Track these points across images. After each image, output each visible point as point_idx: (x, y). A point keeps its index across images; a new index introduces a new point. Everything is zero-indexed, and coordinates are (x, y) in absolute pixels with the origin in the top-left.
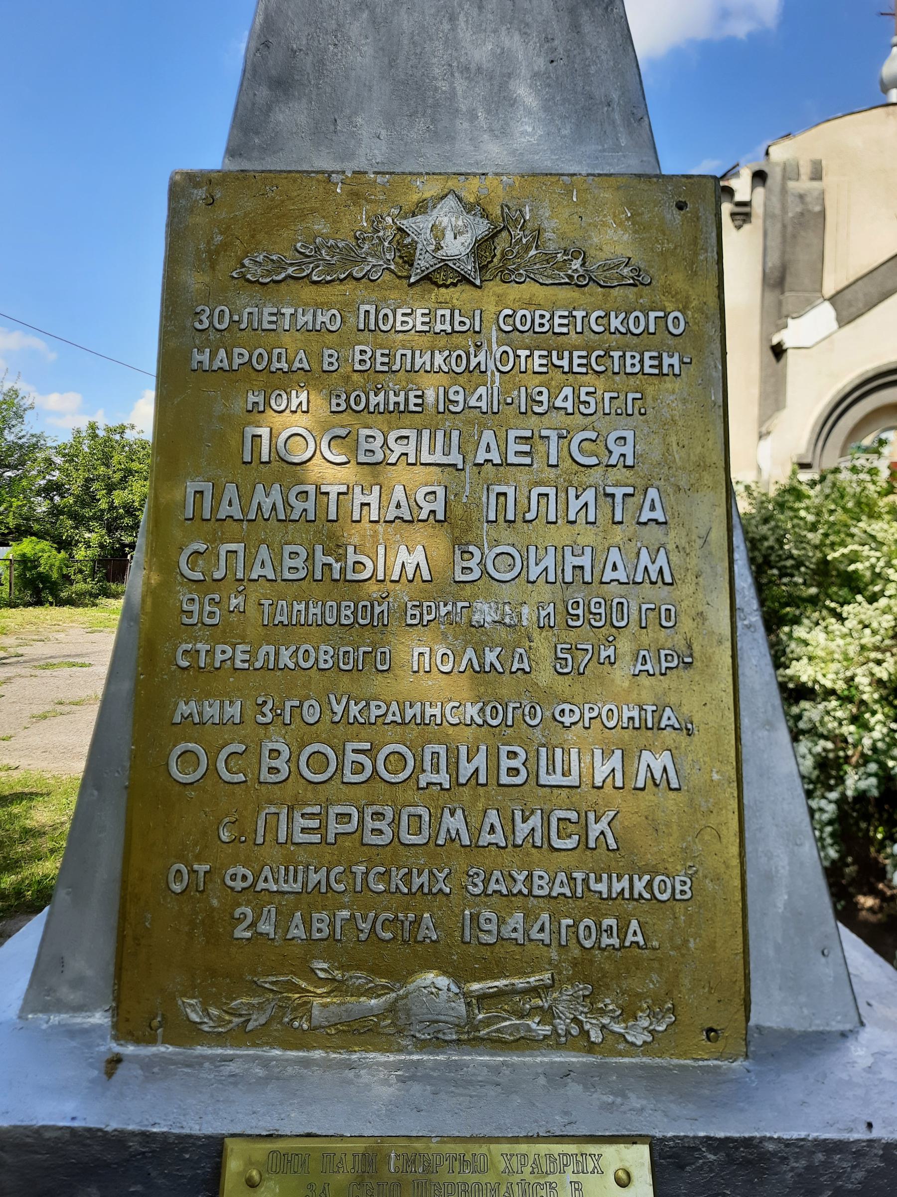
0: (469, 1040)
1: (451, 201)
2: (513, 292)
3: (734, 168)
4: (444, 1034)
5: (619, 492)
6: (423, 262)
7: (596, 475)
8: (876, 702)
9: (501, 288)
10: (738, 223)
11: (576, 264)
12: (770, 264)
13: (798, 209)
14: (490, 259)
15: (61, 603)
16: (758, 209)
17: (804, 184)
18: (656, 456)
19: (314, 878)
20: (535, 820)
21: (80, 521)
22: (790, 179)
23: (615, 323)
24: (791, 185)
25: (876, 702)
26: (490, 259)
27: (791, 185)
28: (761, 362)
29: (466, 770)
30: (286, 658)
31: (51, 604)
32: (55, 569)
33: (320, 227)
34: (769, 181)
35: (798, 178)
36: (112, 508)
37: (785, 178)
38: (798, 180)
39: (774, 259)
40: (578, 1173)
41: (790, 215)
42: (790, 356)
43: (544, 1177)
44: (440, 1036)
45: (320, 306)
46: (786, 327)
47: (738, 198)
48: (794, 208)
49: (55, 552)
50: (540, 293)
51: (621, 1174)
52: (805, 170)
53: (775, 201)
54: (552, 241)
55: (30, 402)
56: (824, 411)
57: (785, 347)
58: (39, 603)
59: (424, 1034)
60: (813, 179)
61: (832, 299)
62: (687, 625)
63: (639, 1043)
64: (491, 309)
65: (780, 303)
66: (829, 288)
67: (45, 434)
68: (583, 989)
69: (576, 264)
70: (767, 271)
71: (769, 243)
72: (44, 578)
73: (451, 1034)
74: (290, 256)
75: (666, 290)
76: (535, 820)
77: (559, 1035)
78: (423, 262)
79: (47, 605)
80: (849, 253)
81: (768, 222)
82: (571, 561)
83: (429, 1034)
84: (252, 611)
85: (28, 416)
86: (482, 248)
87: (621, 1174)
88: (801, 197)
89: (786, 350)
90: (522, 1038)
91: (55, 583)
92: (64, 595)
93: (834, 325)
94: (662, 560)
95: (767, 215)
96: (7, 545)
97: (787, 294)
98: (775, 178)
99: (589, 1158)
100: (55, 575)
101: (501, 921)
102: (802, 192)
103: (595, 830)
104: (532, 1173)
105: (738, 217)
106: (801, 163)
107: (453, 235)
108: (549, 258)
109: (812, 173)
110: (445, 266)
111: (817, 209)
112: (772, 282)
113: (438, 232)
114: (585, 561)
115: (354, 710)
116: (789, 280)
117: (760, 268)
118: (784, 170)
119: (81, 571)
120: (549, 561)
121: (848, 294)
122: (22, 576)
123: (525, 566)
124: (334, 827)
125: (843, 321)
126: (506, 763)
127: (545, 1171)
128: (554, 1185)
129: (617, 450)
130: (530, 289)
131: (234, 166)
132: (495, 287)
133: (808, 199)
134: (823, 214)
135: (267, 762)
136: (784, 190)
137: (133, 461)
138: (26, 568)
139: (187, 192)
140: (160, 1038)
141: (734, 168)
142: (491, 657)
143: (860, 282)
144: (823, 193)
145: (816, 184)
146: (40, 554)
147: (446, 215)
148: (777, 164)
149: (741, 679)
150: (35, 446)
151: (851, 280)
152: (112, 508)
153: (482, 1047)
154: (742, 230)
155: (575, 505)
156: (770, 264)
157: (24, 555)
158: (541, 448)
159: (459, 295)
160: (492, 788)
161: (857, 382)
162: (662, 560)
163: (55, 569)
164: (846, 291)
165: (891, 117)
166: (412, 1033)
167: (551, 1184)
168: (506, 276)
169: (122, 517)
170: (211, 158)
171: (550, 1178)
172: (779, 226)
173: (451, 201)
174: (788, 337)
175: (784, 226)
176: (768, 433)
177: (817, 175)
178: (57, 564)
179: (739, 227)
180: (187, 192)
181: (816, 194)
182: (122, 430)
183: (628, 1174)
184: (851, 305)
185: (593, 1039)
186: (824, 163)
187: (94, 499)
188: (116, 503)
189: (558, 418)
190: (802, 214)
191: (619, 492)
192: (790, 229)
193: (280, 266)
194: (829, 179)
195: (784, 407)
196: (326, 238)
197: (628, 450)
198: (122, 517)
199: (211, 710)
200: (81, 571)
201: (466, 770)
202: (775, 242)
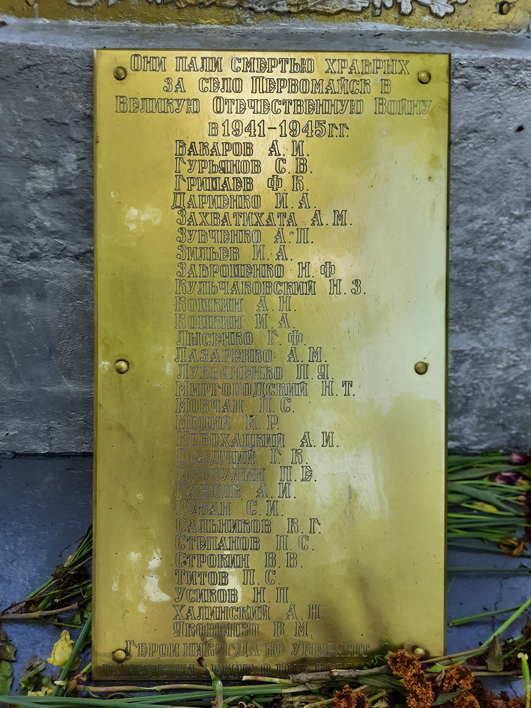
0: (299, 13)
4: (277, 6)
8: (525, 211)
25: (525, 211)
40: (388, 73)
43: (360, 76)
44: (274, 7)
51: (423, 75)
59: (260, 6)
63: (442, 14)
73: (283, 5)
77: (375, 8)
83: (264, 7)
87: (423, 75)
90: (344, 10)
99: (398, 63)
104: (350, 73)
127: (361, 71)
128: (368, 82)
140: (37, 12)
149: (452, 120)
153: (309, 20)
166: (250, 5)
167: (365, 81)
171: (365, 77)
183: (430, 76)
185: (403, 10)
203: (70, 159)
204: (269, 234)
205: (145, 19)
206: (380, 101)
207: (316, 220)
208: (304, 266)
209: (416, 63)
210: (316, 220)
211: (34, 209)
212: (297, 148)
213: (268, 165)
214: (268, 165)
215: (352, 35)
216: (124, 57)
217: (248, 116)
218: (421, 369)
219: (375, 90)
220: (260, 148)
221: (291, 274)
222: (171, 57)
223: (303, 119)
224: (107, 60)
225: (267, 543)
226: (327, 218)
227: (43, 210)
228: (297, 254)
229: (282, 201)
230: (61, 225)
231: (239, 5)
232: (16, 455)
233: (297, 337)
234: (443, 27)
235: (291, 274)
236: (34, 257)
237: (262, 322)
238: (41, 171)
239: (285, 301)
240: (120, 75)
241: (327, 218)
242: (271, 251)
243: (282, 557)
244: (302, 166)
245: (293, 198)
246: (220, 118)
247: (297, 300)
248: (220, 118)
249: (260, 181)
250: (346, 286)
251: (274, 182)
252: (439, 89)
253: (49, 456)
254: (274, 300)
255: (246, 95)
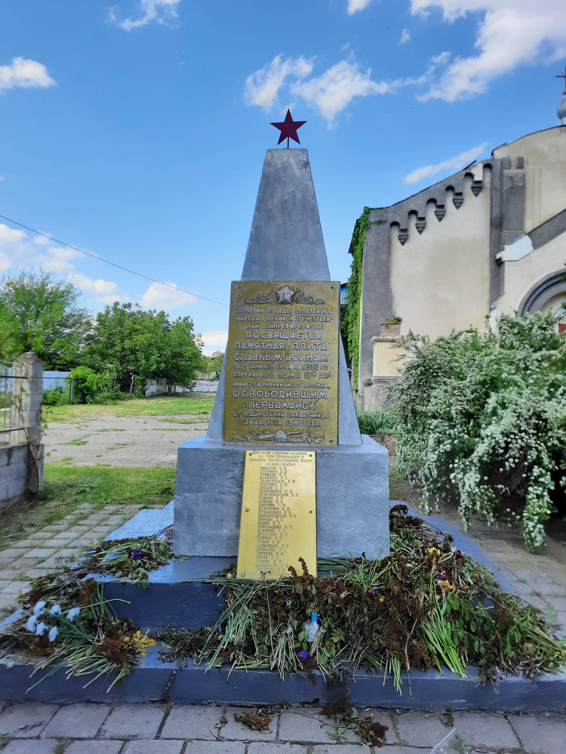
1: (287, 287)
2: (298, 305)
3: (473, 163)
5: (318, 344)
6: (281, 300)
7: (313, 341)
9: (296, 305)
10: (476, 193)
11: (311, 300)
12: (494, 215)
13: (510, 185)
14: (294, 299)
15: (98, 403)
16: (487, 183)
17: (513, 171)
18: (325, 337)
19: (259, 414)
20: (300, 404)
21: (104, 357)
22: (505, 168)
23: (318, 311)
24: (506, 171)
26: (294, 299)
27: (506, 171)
28: (490, 269)
29: (287, 395)
30: (254, 375)
31: (91, 403)
32: (95, 384)
33: (261, 292)
34: (494, 170)
35: (510, 167)
36: (123, 349)
37: (502, 168)
38: (510, 169)
39: (496, 212)
41: (505, 188)
42: (507, 266)
45: (261, 308)
46: (503, 250)
47: (476, 179)
48: (507, 185)
49: (94, 374)
50: (304, 306)
52: (514, 163)
53: (497, 180)
54: (306, 295)
55: (79, 291)
56: (526, 296)
57: (503, 260)
58: (84, 402)
60: (518, 168)
61: (529, 234)
62: (329, 369)
64: (294, 309)
65: (500, 237)
66: (529, 226)
67: (87, 309)
68: (307, 433)
69: (311, 300)
70: (493, 218)
71: (494, 204)
72: (88, 389)
74: (255, 298)
75: (328, 305)
76: (300, 404)
78: (281, 300)
79: (89, 403)
80: (541, 206)
81: (493, 192)
82: (308, 357)
84: (248, 366)
85: (78, 300)
86: (292, 297)
88: (511, 178)
89: (503, 262)
91: (94, 392)
92: (98, 398)
93: (531, 248)
94: (325, 357)
95: (492, 188)
96: (69, 371)
97: (504, 231)
98: (497, 167)
100: (95, 388)
101: (293, 422)
102: (512, 175)
103: (311, 406)
105: (476, 189)
106: (512, 159)
107: (286, 294)
108: (306, 298)
109: (518, 164)
110: (285, 300)
111: (521, 184)
112: (496, 224)
113: (284, 294)
114: (311, 357)
115: (267, 385)
116: (505, 223)
117: (489, 217)
118: (502, 163)
119: (106, 385)
120: (304, 357)
121: (539, 231)
122: (76, 387)
123: (299, 358)
124: (263, 405)
125: (536, 245)
126: (295, 394)
129: (318, 336)
130: (302, 304)
131: (244, 280)
132: (295, 304)
133: (516, 179)
134: (523, 187)
135: (251, 394)
136: (501, 174)
137: (135, 323)
138: (78, 383)
139: (234, 284)
141: (473, 163)
142: (292, 375)
143: (546, 225)
144: (524, 175)
145: (520, 171)
146: (86, 375)
147: (286, 290)
148: (498, 160)
150: (189, 317)
151: (542, 223)
152: (123, 349)
154: (479, 196)
155: (309, 346)
156: (494, 215)
157: (77, 376)
158: (303, 335)
159: (288, 306)
160: (292, 398)
161: (545, 280)
162: (325, 357)
163: (95, 384)
164: (538, 230)
165: (563, 133)
168: (297, 302)
169: (128, 355)
170: (238, 278)
172: (499, 194)
173: (287, 287)
174: (506, 254)
175: (502, 194)
176: (495, 308)
177: (521, 164)
178: (96, 381)
179: (476, 195)
180: (234, 284)
181: (520, 176)
182: (129, 306)
184: (541, 236)
186: (525, 158)
187: (113, 345)
188: (126, 346)
189: (306, 330)
190: (512, 187)
191: (318, 344)
192: (505, 196)
193: (253, 300)
194: (529, 168)
195: (503, 294)
196: (262, 295)
197: (320, 336)
198: (128, 355)
199: (240, 384)
200: (106, 385)
201: (287, 395)
202: (496, 203)
203: (237, 471)
204: (279, 484)
205: (255, 443)
206: (302, 460)
207: (289, 481)
208: (286, 491)
209: (309, 453)
210: (289, 481)
211: (226, 482)
212: (285, 468)
213: (279, 471)
214: (279, 471)
215: (298, 447)
216: (252, 452)
217: (275, 462)
218: (311, 512)
219: (301, 458)
220: (278, 468)
221: (283, 492)
222: (260, 452)
223: (286, 463)
224: (248, 452)
225: (277, 550)
226: (291, 481)
227: (229, 482)
228: (284, 488)
229: (282, 478)
230: (232, 485)
231: (186, 742)
232: (205, 557)
233: (284, 505)
234: (318, 445)
235: (283, 492)
236: (224, 493)
237: (277, 502)
238: (230, 473)
239: (282, 498)
240: (250, 454)
241: (291, 481)
242: (279, 489)
243: (280, 553)
244: (286, 472)
245: (284, 478)
246: (270, 463)
247: (284, 497)
248: (270, 463)
249: (277, 474)
250: (295, 495)
251: (280, 474)
252: (314, 457)
253: (214, 557)
254: (279, 497)
255: (275, 458)
